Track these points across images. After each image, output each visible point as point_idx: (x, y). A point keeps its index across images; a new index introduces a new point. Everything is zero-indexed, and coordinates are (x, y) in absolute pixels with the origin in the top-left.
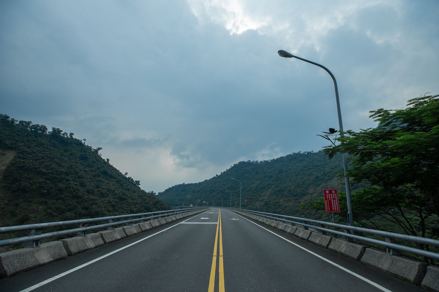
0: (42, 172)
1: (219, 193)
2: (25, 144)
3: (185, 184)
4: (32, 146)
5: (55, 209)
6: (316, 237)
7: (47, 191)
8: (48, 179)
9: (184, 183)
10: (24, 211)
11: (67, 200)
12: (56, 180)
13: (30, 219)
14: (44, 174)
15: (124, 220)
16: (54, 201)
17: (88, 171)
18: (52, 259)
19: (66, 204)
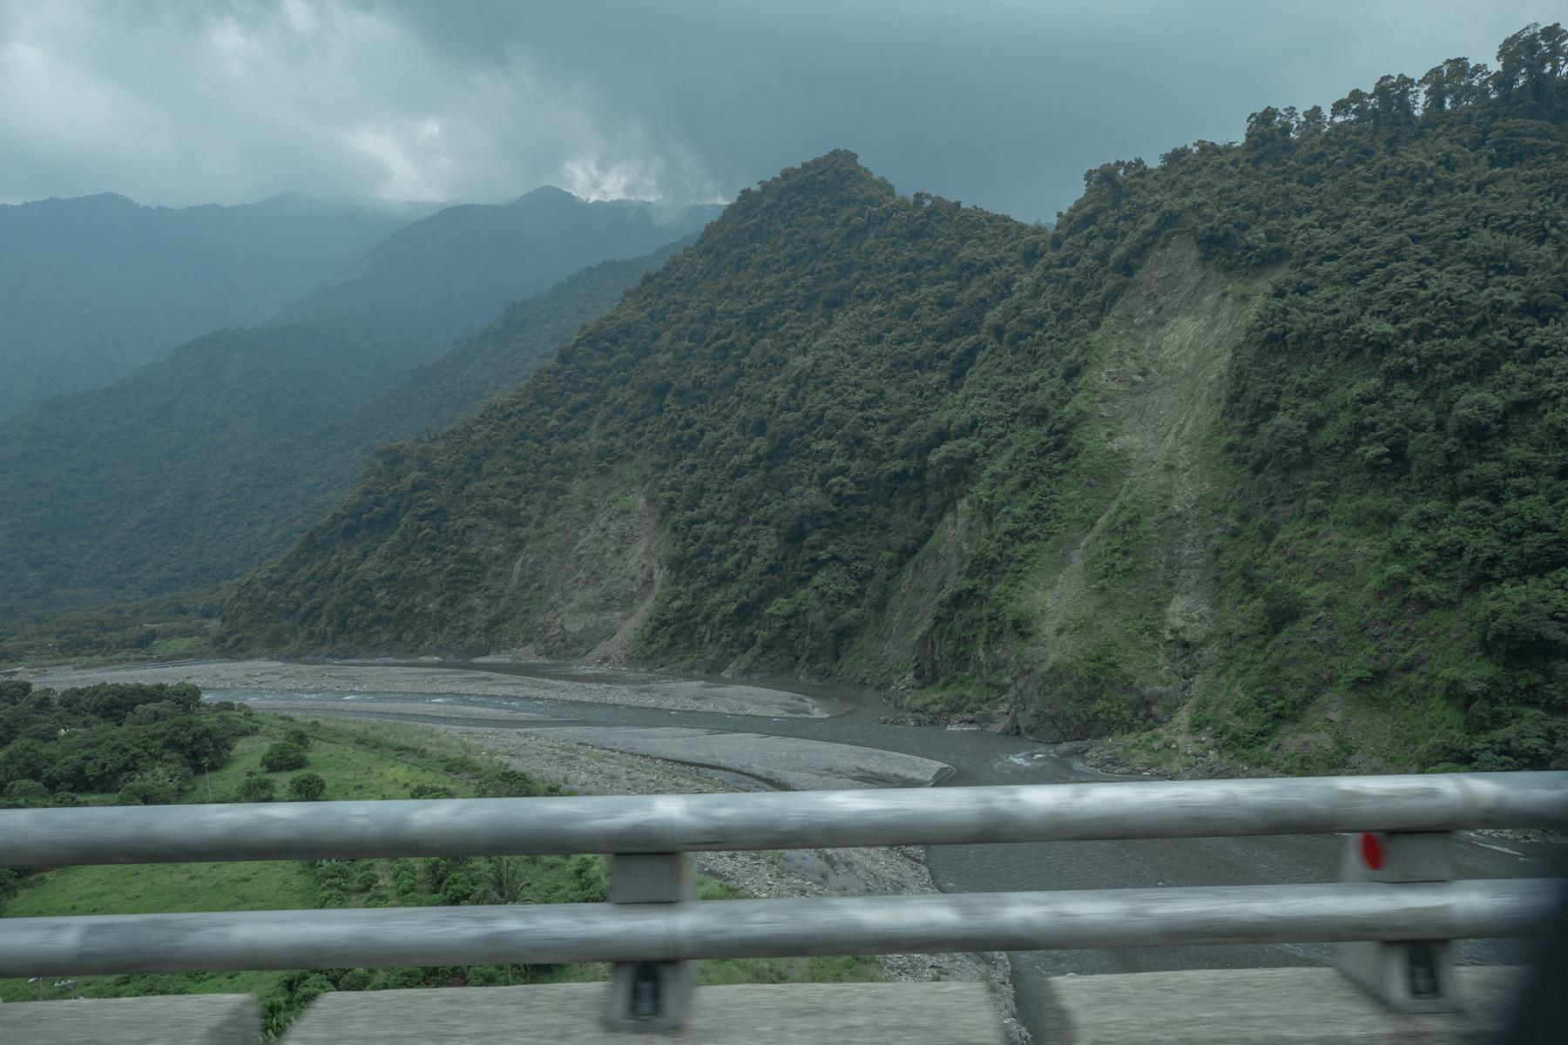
0: (1368, 343)
1: (239, 603)
2: (1326, 211)
3: (963, 206)
4: (1530, 141)
5: (1431, 555)
6: (247, 571)
7: (1387, 450)
8: (1406, 373)
9: (1558, 24)
10: (1290, 567)
11: (1522, 494)
12: (1442, 372)
13: (1306, 614)
14: (1382, 347)
15: (897, 888)
16: (1423, 507)
17: (885, 449)
18: (48, 876)
19: (1510, 520)
